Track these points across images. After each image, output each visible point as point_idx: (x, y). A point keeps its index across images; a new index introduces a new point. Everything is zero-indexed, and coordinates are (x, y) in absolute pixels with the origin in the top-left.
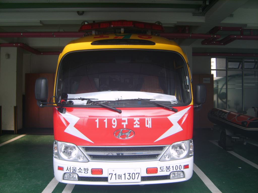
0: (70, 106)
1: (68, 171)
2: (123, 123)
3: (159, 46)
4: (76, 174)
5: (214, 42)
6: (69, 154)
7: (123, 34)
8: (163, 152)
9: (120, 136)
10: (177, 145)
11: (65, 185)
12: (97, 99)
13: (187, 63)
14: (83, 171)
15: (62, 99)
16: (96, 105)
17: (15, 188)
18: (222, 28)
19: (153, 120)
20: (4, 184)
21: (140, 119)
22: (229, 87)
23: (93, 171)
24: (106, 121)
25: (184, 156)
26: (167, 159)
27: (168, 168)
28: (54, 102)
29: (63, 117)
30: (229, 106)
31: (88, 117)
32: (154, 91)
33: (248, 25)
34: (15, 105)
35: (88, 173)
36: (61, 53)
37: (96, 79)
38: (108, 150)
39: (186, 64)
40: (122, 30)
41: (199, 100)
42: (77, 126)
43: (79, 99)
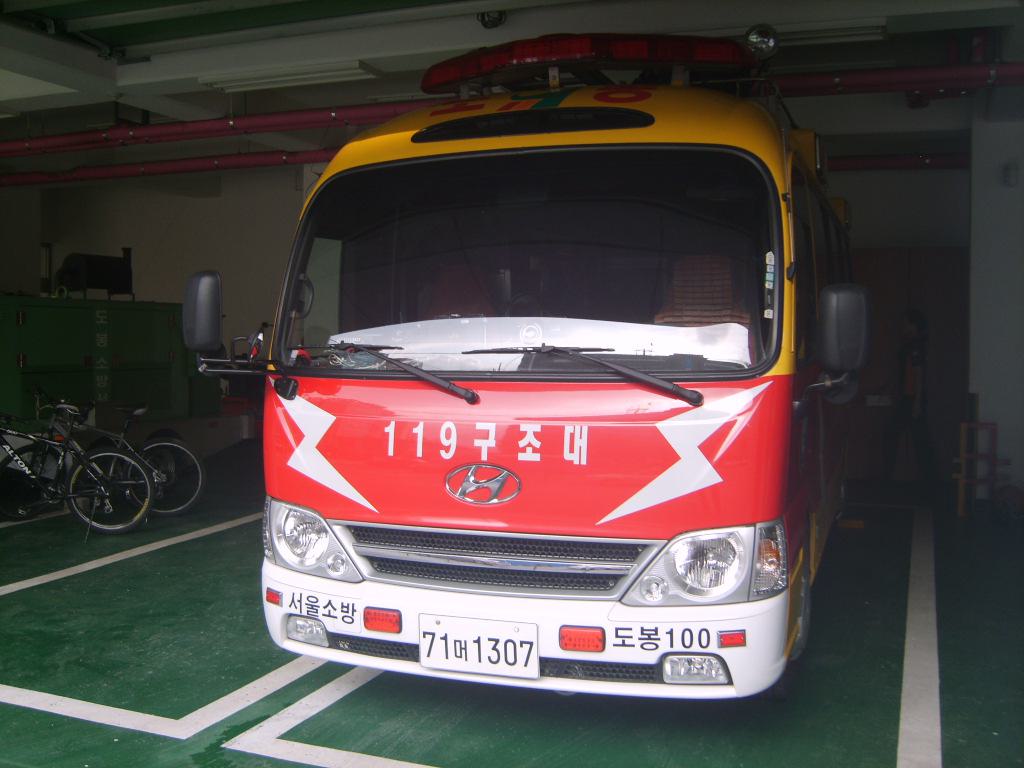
8: (634, 568)
12: (609, 347)
13: (784, 196)
14: (339, 614)
21: (543, 427)
23: (373, 617)
24: (419, 431)
27: (649, 635)
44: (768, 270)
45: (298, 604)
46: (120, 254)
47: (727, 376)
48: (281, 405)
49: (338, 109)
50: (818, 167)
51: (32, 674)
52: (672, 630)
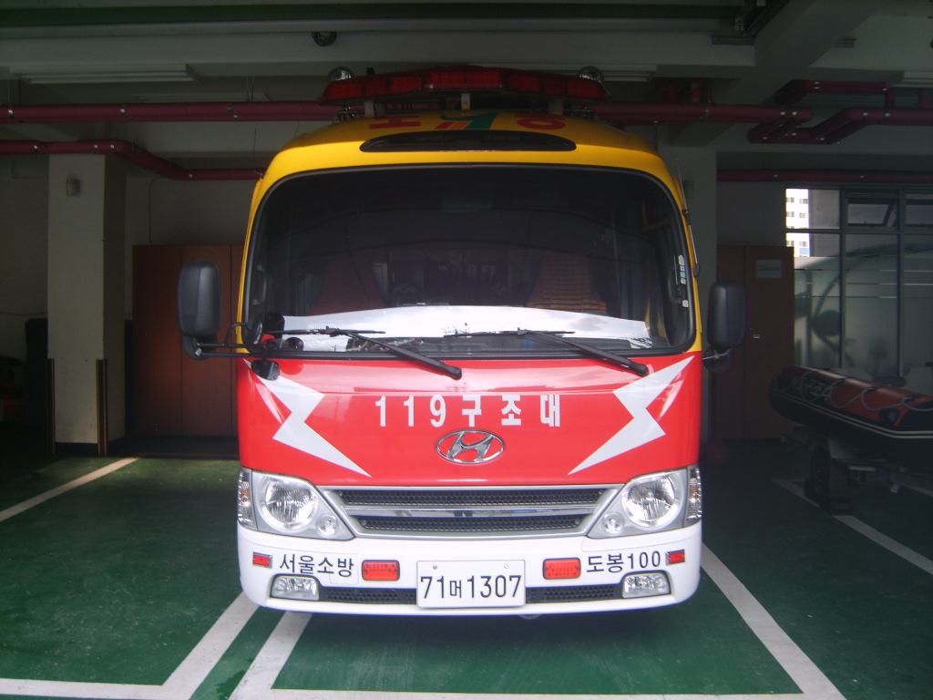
0: (291, 357)
1: (284, 570)
2: (465, 412)
3: (588, 153)
4: (313, 581)
5: (794, 134)
6: (288, 515)
7: (468, 115)
8: (598, 509)
9: (455, 454)
10: (647, 483)
11: (277, 615)
13: (684, 211)
14: (336, 569)
15: (265, 331)
16: (378, 351)
17: (111, 627)
18: (816, 86)
19: (566, 403)
20: (75, 615)
22: (849, 291)
23: (370, 569)
24: (410, 403)
25: (670, 522)
26: (612, 530)
28: (240, 341)
29: (268, 390)
30: (849, 359)
31: (353, 391)
32: (575, 307)
33: (907, 75)
34: (101, 357)
35: (350, 574)
36: (261, 180)
37: (379, 264)
38: (417, 499)
39: (679, 214)
40: (466, 100)
41: (722, 334)
42: (315, 421)
49: (127, 106)
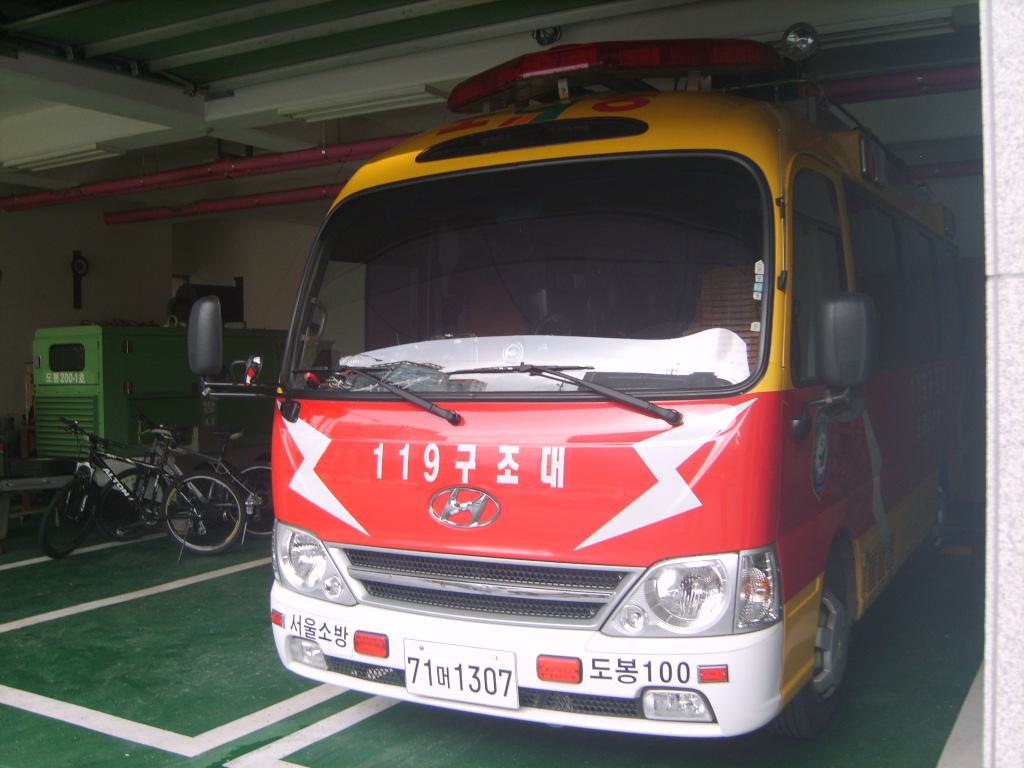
8: (616, 595)
13: (778, 200)
14: (333, 637)
27: (626, 667)
43: (516, 370)
44: (757, 280)
45: (297, 626)
46: (233, 284)
47: (707, 389)
48: (284, 426)
50: (864, 170)
51: (77, 688)
52: (429, 661)
